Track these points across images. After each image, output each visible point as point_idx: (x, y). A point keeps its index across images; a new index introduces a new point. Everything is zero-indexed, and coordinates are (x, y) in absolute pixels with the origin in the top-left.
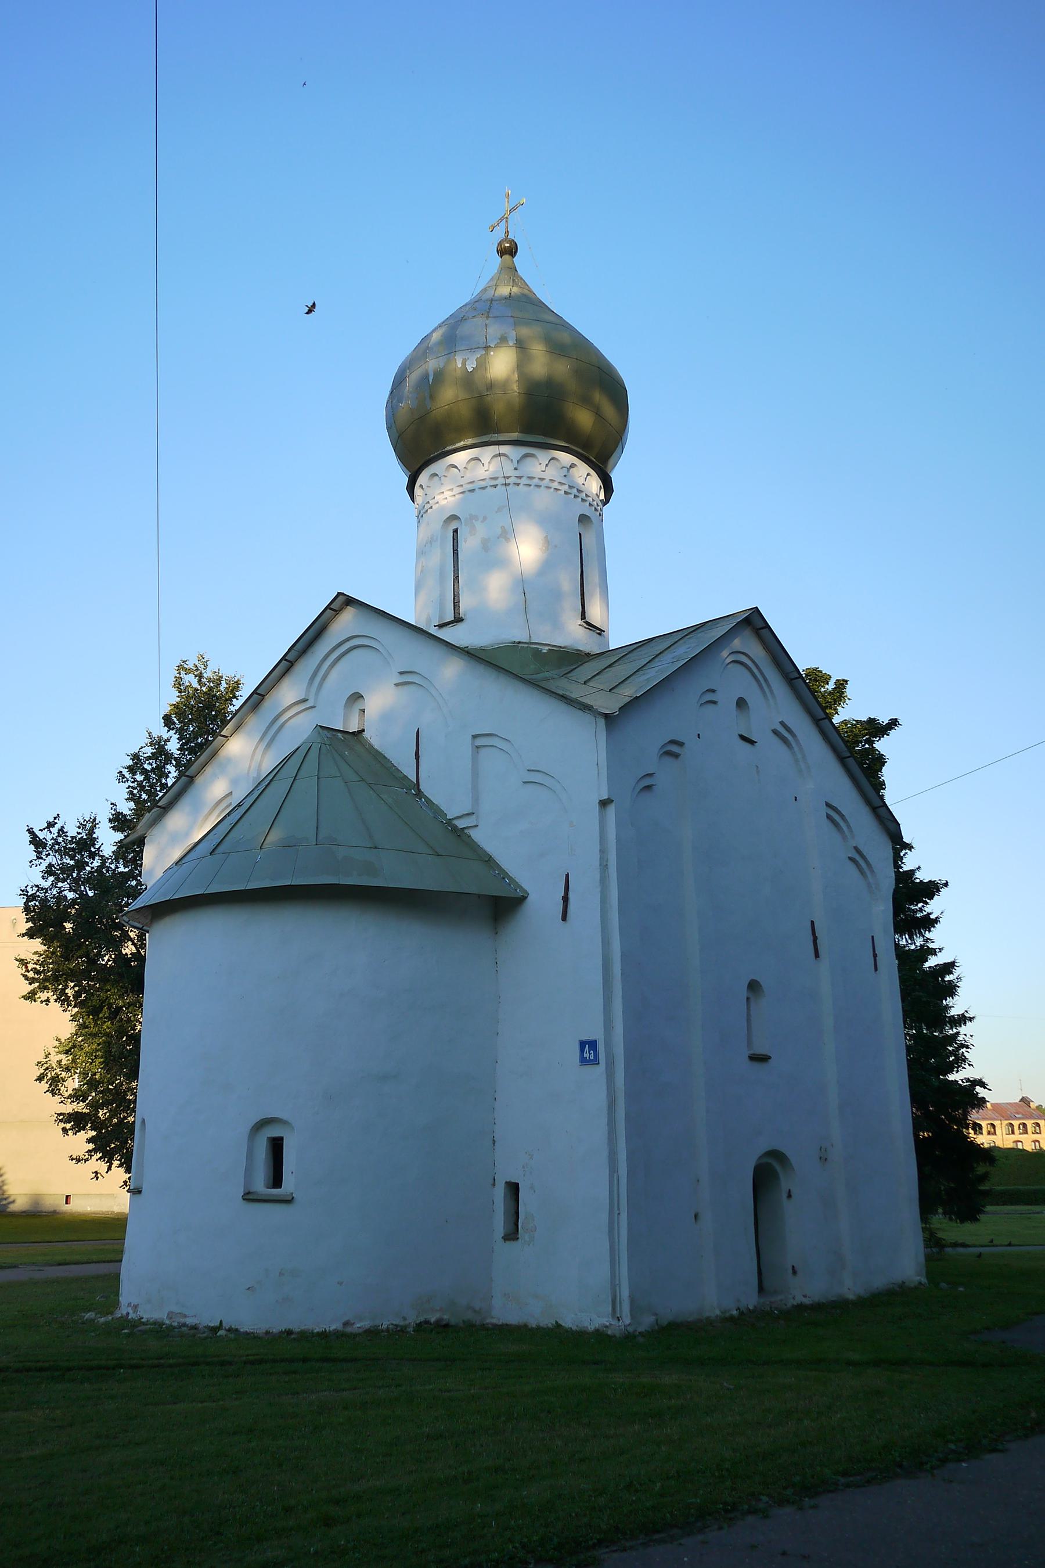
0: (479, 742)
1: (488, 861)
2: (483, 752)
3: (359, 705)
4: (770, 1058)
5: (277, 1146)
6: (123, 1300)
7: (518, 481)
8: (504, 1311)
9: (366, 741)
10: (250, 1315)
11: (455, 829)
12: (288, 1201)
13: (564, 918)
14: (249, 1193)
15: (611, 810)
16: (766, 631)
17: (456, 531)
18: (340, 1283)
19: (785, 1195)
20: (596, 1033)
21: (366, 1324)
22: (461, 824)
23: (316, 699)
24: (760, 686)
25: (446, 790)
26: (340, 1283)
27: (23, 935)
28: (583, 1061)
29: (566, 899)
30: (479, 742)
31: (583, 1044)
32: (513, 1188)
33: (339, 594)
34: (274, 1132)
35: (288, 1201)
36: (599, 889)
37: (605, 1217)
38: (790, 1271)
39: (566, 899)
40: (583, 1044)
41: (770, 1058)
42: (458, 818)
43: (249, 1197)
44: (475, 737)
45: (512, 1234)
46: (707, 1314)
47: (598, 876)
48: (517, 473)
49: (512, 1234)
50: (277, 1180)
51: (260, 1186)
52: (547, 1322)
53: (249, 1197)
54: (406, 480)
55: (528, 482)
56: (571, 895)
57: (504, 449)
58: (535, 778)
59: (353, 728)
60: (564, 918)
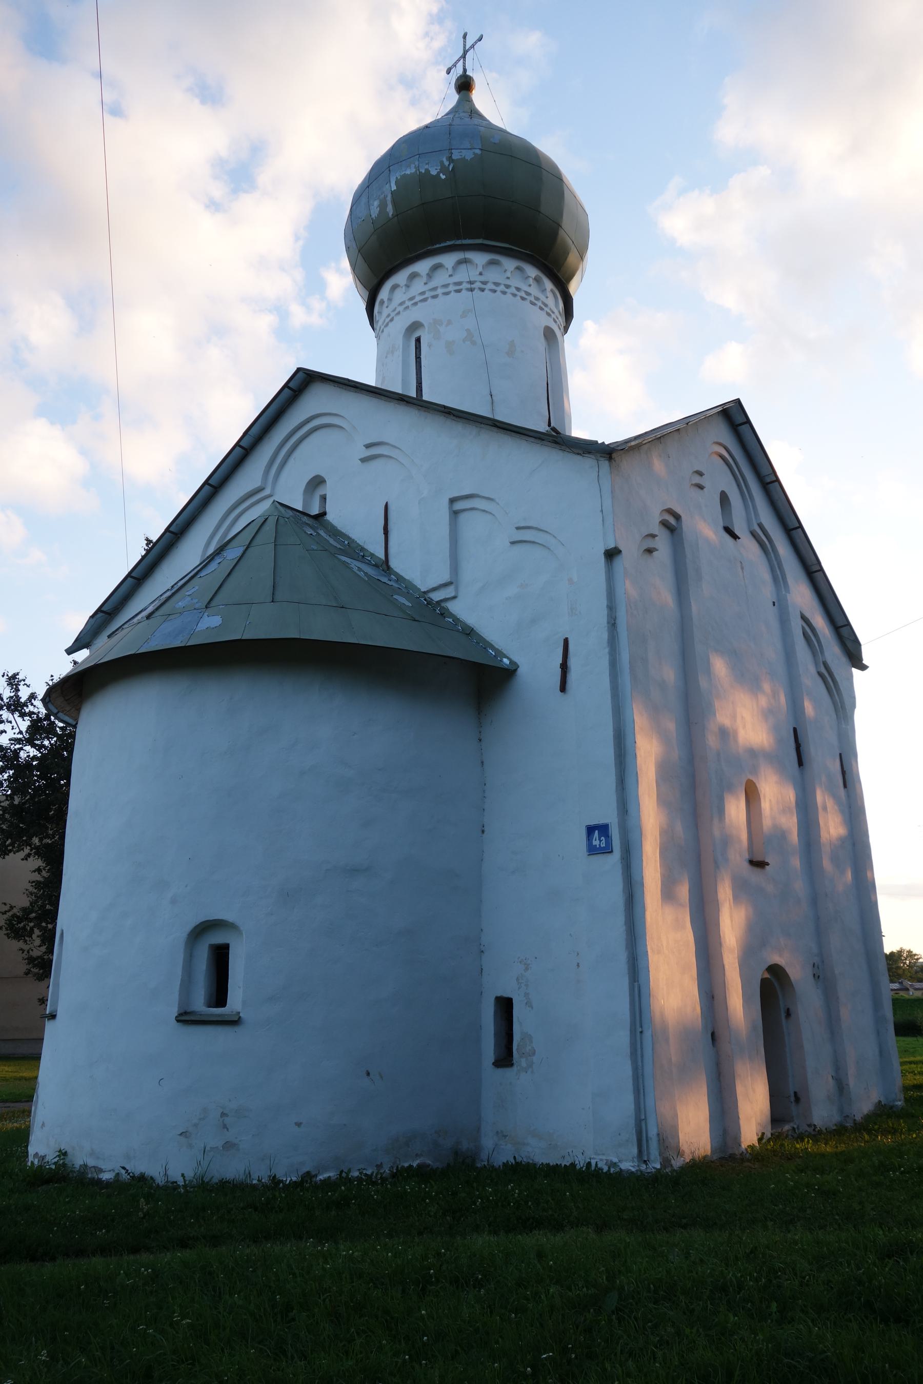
0: (459, 506)
1: (469, 632)
2: (463, 517)
3: (320, 492)
4: (768, 864)
5: (221, 956)
6: (31, 1150)
7: (483, 286)
8: (538, 1153)
9: (329, 523)
10: (174, 1164)
11: (430, 602)
12: (234, 1022)
13: (563, 688)
14: (186, 1013)
15: (620, 563)
16: (748, 425)
17: (418, 340)
18: (299, 1124)
19: (783, 1015)
20: (608, 815)
21: (332, 1174)
22: (436, 596)
23: (273, 488)
24: (739, 486)
25: (418, 562)
26: (299, 1124)
27: (34, 871)
28: (592, 850)
29: (564, 667)
30: (456, 508)
31: (590, 830)
32: (505, 1006)
33: (299, 370)
34: (218, 938)
35: (234, 1022)
36: (607, 650)
37: (623, 1037)
38: (793, 1099)
39: (564, 667)
40: (590, 830)
41: (768, 864)
42: (434, 589)
43: (186, 1018)
44: (452, 501)
45: (505, 1058)
46: (731, 1151)
47: (605, 636)
48: (482, 278)
49: (505, 1058)
50: (219, 996)
51: (199, 1004)
52: (567, 1162)
53: (186, 1018)
54: (363, 306)
55: (494, 287)
56: (573, 662)
57: (470, 255)
58: (526, 536)
59: (315, 511)
60: (563, 688)
